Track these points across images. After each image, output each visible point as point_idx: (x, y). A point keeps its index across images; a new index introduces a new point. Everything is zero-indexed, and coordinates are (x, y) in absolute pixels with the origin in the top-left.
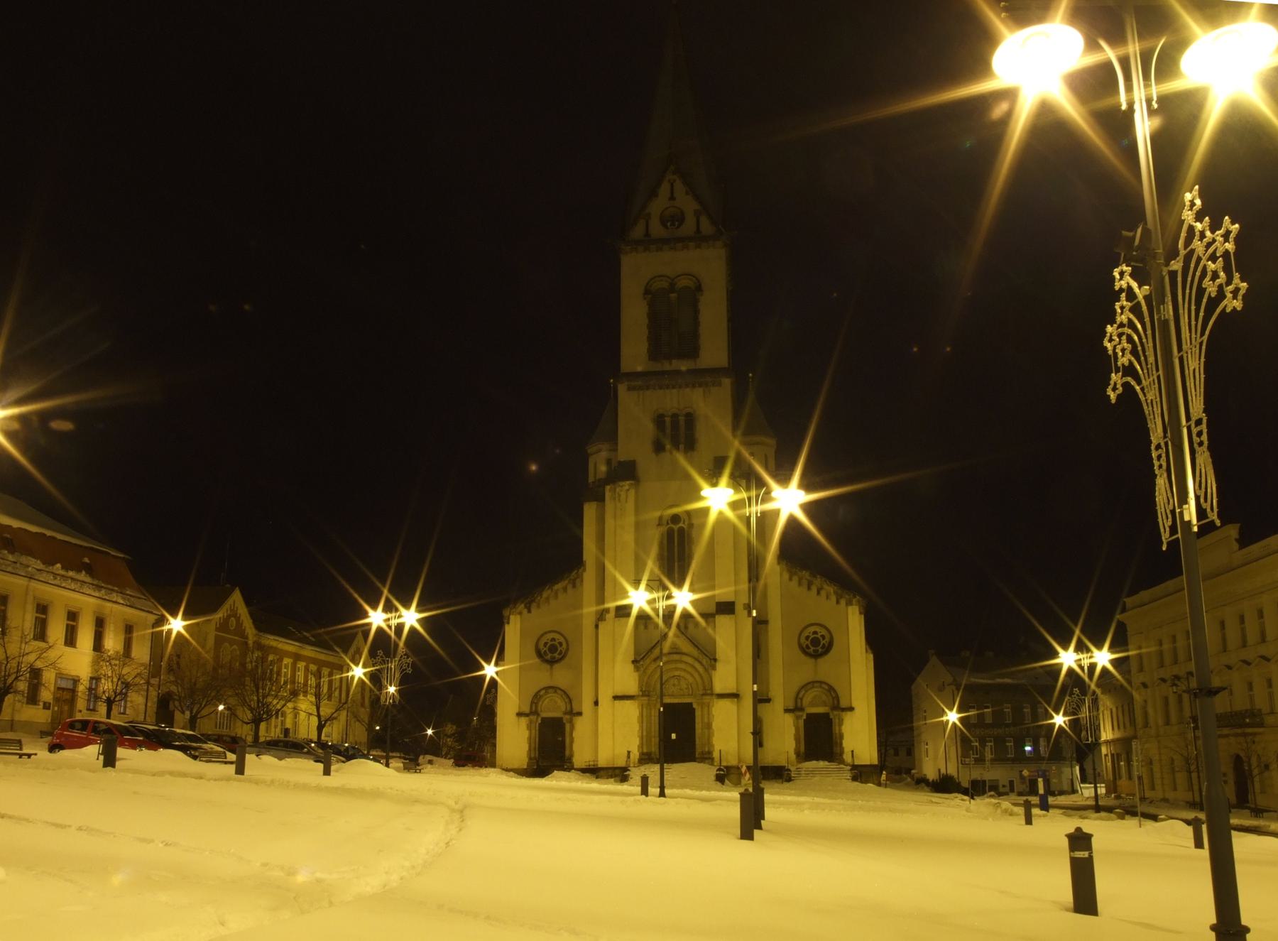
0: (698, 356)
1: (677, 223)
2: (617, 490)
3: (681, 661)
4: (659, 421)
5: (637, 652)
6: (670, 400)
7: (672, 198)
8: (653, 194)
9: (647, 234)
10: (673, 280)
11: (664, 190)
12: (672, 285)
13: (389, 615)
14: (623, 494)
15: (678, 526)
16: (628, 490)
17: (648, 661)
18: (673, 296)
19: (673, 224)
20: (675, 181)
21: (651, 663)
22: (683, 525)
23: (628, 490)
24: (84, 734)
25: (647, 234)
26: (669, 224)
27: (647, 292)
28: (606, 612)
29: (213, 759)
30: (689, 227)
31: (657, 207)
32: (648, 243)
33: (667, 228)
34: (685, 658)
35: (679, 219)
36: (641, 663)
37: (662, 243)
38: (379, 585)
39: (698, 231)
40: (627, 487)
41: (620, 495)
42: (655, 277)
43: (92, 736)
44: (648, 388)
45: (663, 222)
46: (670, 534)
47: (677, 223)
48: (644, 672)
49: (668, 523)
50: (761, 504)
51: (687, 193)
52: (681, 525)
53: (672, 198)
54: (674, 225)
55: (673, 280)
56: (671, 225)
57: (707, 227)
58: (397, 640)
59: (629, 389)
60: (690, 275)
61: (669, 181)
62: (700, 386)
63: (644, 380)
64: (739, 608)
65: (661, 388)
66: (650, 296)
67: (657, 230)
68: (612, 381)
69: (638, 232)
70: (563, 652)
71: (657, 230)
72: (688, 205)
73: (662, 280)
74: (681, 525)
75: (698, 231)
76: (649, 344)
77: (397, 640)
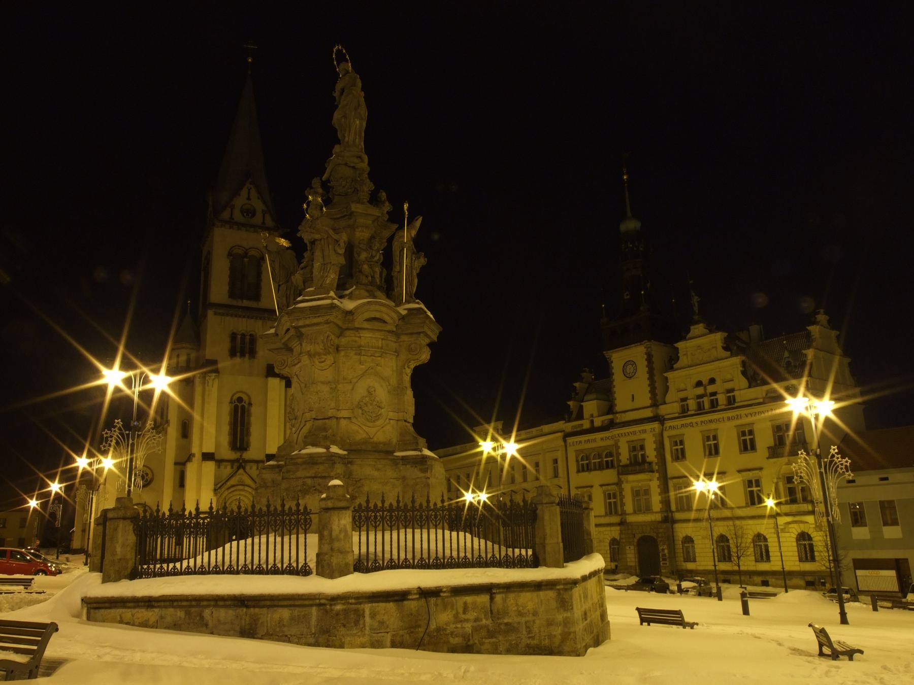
0: (260, 301)
1: (250, 215)
2: (207, 378)
3: (244, 490)
4: (233, 336)
5: (215, 485)
6: (243, 325)
7: (249, 199)
8: (237, 193)
9: (231, 217)
10: (247, 250)
11: (244, 192)
12: (246, 253)
13: (92, 460)
14: (210, 383)
15: (241, 404)
16: (214, 379)
17: (223, 489)
18: (246, 260)
19: (248, 215)
20: (251, 188)
21: (225, 491)
22: (244, 404)
23: (214, 379)
24: (4, 560)
25: (231, 217)
26: (245, 214)
27: (230, 254)
28: (193, 456)
29: (636, 503)
30: (258, 219)
31: (240, 201)
32: (232, 223)
33: (243, 215)
34: (247, 488)
35: (251, 213)
36: (219, 491)
37: (240, 225)
38: (81, 439)
39: (264, 223)
40: (213, 377)
41: (208, 382)
42: (235, 246)
43: (12, 561)
44: (227, 315)
45: (242, 212)
46: (236, 407)
47: (250, 215)
48: (220, 496)
49: (235, 402)
50: (142, 385)
51: (258, 198)
52: (243, 404)
53: (249, 199)
54: (249, 216)
55: (247, 250)
56: (246, 215)
57: (269, 222)
58: (502, 462)
59: (215, 314)
60: (258, 249)
61: (248, 188)
62: (260, 319)
63: (224, 309)
64: (198, 456)
65: (236, 316)
66: (231, 257)
67: (238, 216)
68: (189, 302)
69: (226, 215)
70: (149, 480)
71: (238, 216)
72: (259, 206)
73: (239, 249)
74: (243, 404)
75: (264, 223)
76: (229, 288)
77: (502, 462)
